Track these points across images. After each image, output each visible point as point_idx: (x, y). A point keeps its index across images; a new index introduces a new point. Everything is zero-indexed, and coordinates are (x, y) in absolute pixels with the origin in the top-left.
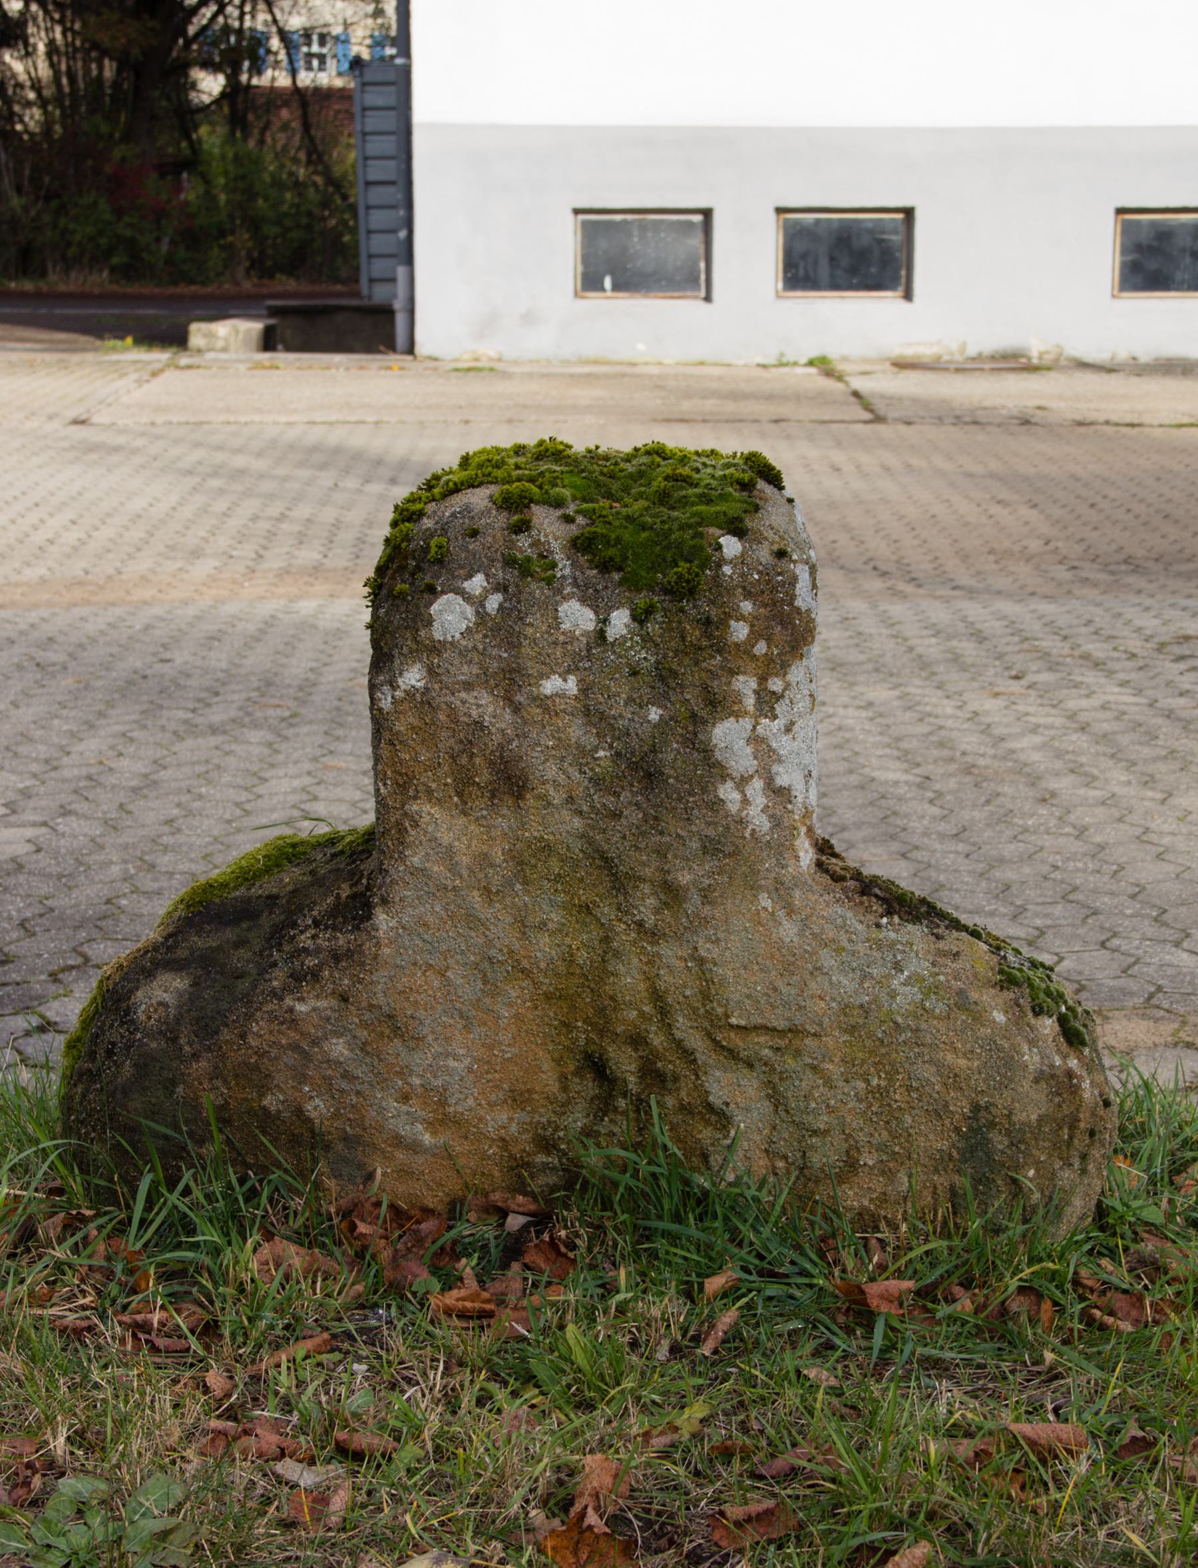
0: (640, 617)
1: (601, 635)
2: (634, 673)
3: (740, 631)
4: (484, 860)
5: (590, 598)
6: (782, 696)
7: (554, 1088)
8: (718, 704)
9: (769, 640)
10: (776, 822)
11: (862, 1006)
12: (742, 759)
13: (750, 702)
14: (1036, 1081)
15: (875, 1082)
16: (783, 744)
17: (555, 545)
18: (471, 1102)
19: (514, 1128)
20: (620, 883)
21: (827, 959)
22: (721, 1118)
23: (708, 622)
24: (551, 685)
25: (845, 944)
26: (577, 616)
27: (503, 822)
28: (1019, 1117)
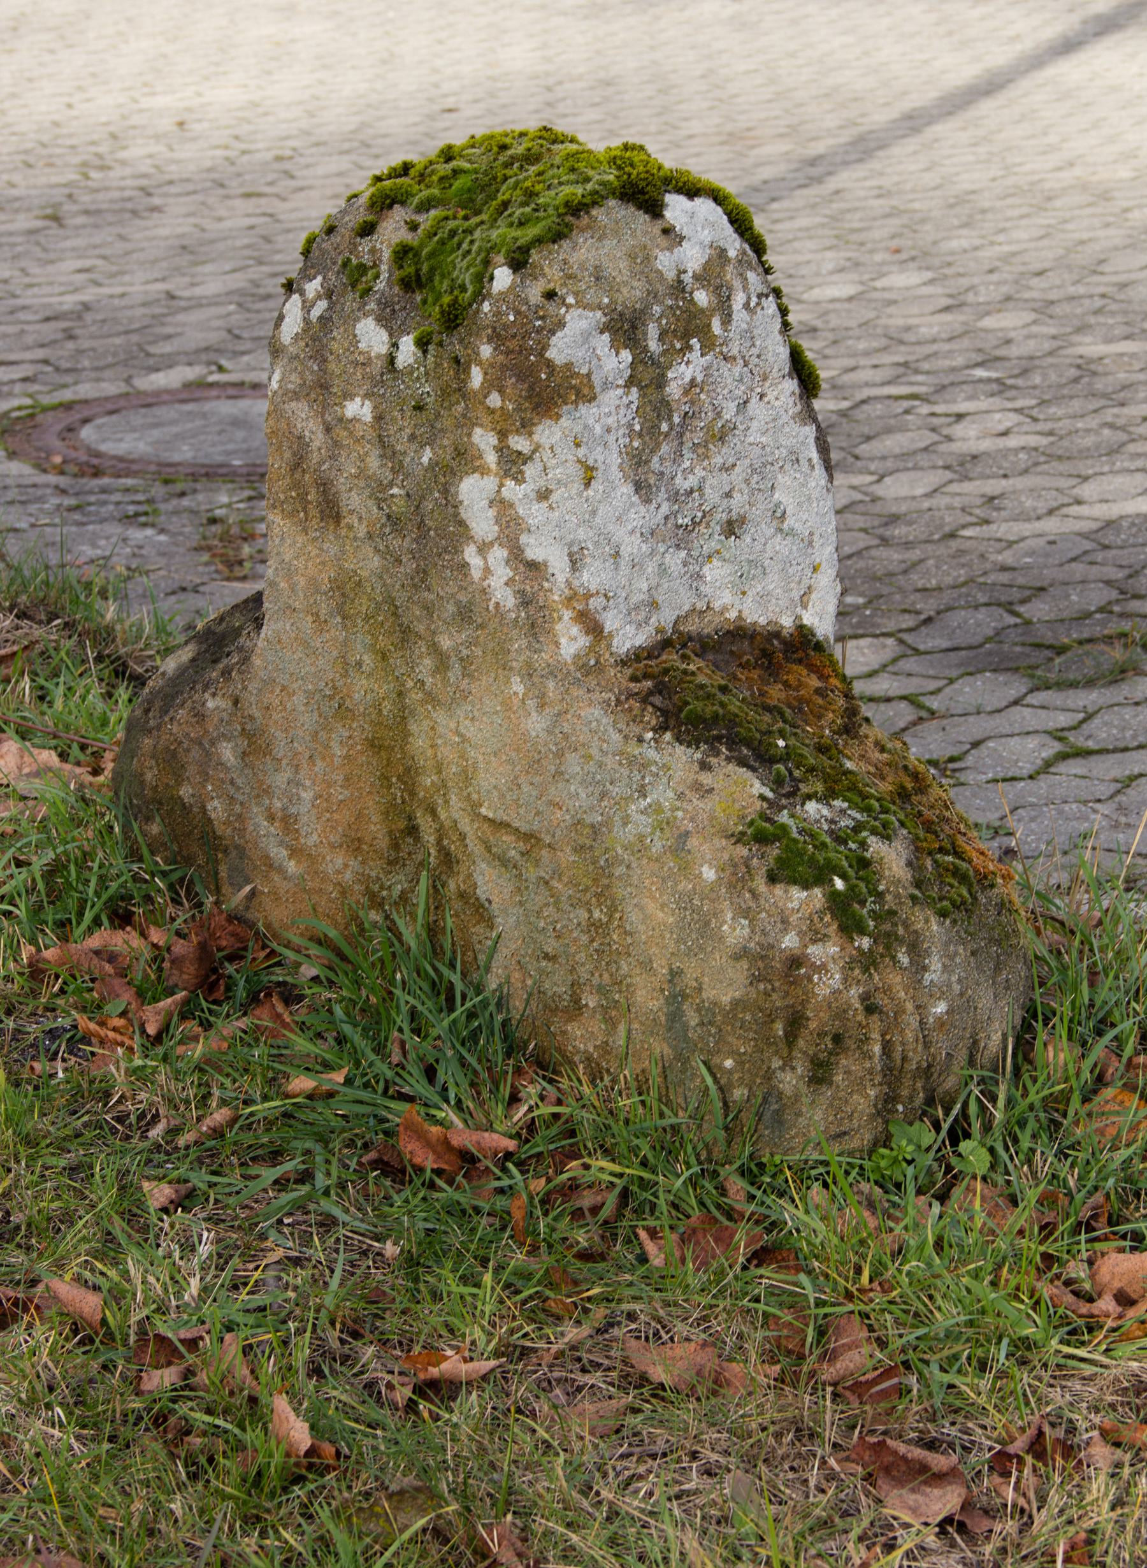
0: (423, 344)
1: (391, 360)
2: (419, 408)
3: (476, 378)
5: (385, 319)
6: (530, 458)
7: (383, 843)
8: (464, 459)
9: (501, 391)
10: (526, 601)
11: (593, 826)
12: (482, 522)
13: (491, 458)
14: (737, 957)
15: (597, 914)
16: (534, 513)
18: (315, 837)
19: (348, 876)
20: (406, 635)
21: (573, 764)
22: (481, 912)
23: (457, 361)
25: (594, 752)
26: (372, 336)
27: (331, 548)
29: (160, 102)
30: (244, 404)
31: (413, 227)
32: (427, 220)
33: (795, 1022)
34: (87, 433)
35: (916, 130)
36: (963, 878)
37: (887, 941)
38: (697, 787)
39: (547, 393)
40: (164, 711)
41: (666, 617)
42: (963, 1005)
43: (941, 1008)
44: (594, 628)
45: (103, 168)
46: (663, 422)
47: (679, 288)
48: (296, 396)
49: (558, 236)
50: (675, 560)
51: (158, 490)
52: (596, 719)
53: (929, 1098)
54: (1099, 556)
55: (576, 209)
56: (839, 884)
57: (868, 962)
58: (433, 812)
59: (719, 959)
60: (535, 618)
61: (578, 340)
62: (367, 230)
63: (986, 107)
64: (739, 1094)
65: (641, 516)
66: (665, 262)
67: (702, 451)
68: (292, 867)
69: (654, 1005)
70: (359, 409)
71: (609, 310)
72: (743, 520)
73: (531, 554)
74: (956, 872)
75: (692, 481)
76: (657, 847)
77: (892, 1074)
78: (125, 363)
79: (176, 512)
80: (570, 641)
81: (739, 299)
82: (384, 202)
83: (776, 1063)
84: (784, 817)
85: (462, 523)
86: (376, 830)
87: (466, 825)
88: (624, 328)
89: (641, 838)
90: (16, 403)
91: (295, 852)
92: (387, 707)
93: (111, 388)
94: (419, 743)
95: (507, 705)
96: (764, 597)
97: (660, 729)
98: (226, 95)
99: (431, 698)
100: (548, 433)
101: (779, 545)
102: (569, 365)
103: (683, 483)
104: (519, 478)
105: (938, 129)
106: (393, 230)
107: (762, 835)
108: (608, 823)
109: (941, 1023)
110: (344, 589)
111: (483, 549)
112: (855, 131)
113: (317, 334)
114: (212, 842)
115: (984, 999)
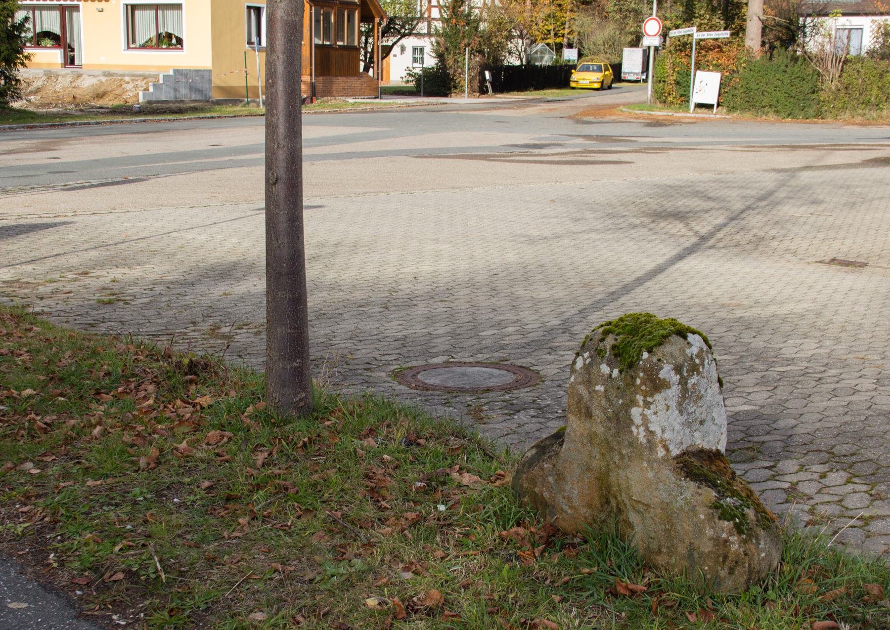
0: (621, 372)
1: (610, 375)
2: (618, 388)
3: (638, 381)
4: (582, 435)
7: (599, 506)
8: (633, 403)
10: (649, 441)
12: (638, 420)
13: (641, 403)
14: (710, 540)
16: (653, 418)
17: (608, 347)
20: (611, 449)
21: (661, 486)
22: (630, 525)
24: (598, 388)
26: (605, 369)
27: (588, 425)
28: (702, 549)
29: (406, 270)
30: (463, 368)
31: (616, 340)
32: (620, 338)
33: (725, 558)
34: (419, 376)
35: (641, 284)
36: (768, 520)
37: (750, 536)
38: (697, 493)
39: (657, 385)
40: (529, 467)
41: (684, 447)
42: (769, 554)
43: (763, 555)
44: (666, 448)
45: (396, 292)
46: (687, 394)
47: (691, 358)
48: (580, 384)
49: (660, 344)
50: (687, 431)
51: (449, 396)
52: (668, 475)
53: (756, 578)
54: (736, 423)
55: (665, 337)
56: (737, 520)
57: (745, 542)
58: (616, 498)
59: (705, 540)
60: (651, 446)
61: (667, 372)
62: (602, 340)
63: (660, 277)
64: (708, 576)
65: (681, 419)
66: (688, 351)
67: (695, 402)
68: (569, 511)
69: (684, 552)
70: (600, 388)
71: (675, 364)
72: (704, 420)
73: (651, 429)
74: (766, 518)
75: (692, 410)
76: (686, 509)
77: (750, 572)
78: (424, 355)
79: (457, 403)
80: (661, 452)
81: (706, 362)
82: (606, 333)
83: (719, 568)
84: (722, 502)
85: (631, 420)
86: (597, 502)
87: (626, 501)
88: (678, 369)
89: (681, 506)
90: (396, 367)
91: (570, 507)
92: (603, 468)
93: (422, 363)
94: (613, 478)
95: (642, 469)
96: (708, 442)
97: (686, 477)
98: (426, 268)
99: (618, 467)
100: (658, 397)
101: (714, 428)
102: (664, 379)
103: (690, 410)
104: (649, 409)
105: (648, 284)
106: (610, 341)
107: (716, 506)
108: (671, 502)
109: (763, 559)
110: (592, 437)
111: (638, 427)
112: (622, 284)
113: (587, 368)
114: (545, 504)
115: (774, 552)
